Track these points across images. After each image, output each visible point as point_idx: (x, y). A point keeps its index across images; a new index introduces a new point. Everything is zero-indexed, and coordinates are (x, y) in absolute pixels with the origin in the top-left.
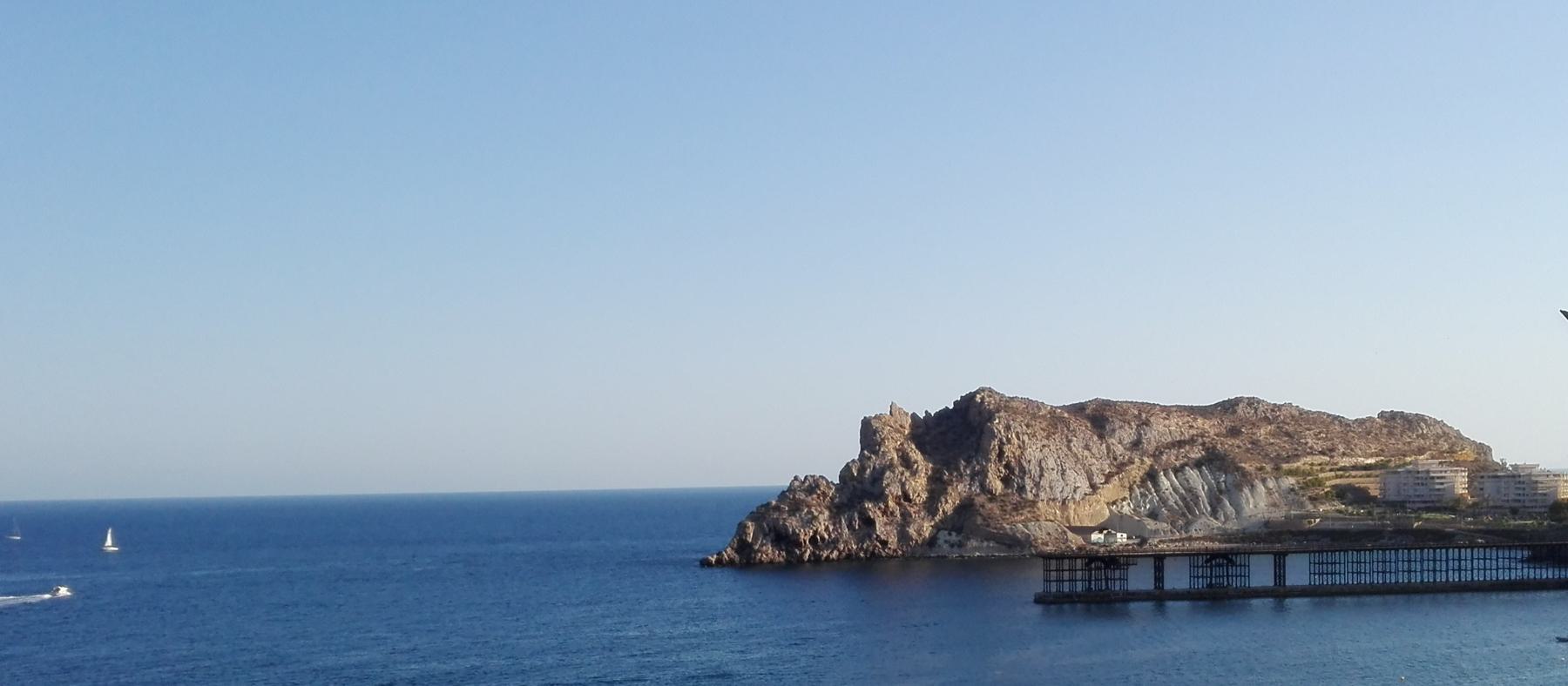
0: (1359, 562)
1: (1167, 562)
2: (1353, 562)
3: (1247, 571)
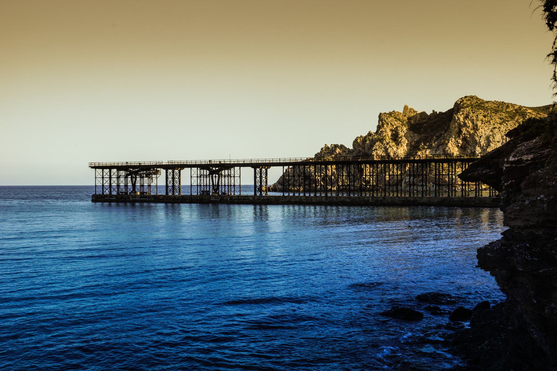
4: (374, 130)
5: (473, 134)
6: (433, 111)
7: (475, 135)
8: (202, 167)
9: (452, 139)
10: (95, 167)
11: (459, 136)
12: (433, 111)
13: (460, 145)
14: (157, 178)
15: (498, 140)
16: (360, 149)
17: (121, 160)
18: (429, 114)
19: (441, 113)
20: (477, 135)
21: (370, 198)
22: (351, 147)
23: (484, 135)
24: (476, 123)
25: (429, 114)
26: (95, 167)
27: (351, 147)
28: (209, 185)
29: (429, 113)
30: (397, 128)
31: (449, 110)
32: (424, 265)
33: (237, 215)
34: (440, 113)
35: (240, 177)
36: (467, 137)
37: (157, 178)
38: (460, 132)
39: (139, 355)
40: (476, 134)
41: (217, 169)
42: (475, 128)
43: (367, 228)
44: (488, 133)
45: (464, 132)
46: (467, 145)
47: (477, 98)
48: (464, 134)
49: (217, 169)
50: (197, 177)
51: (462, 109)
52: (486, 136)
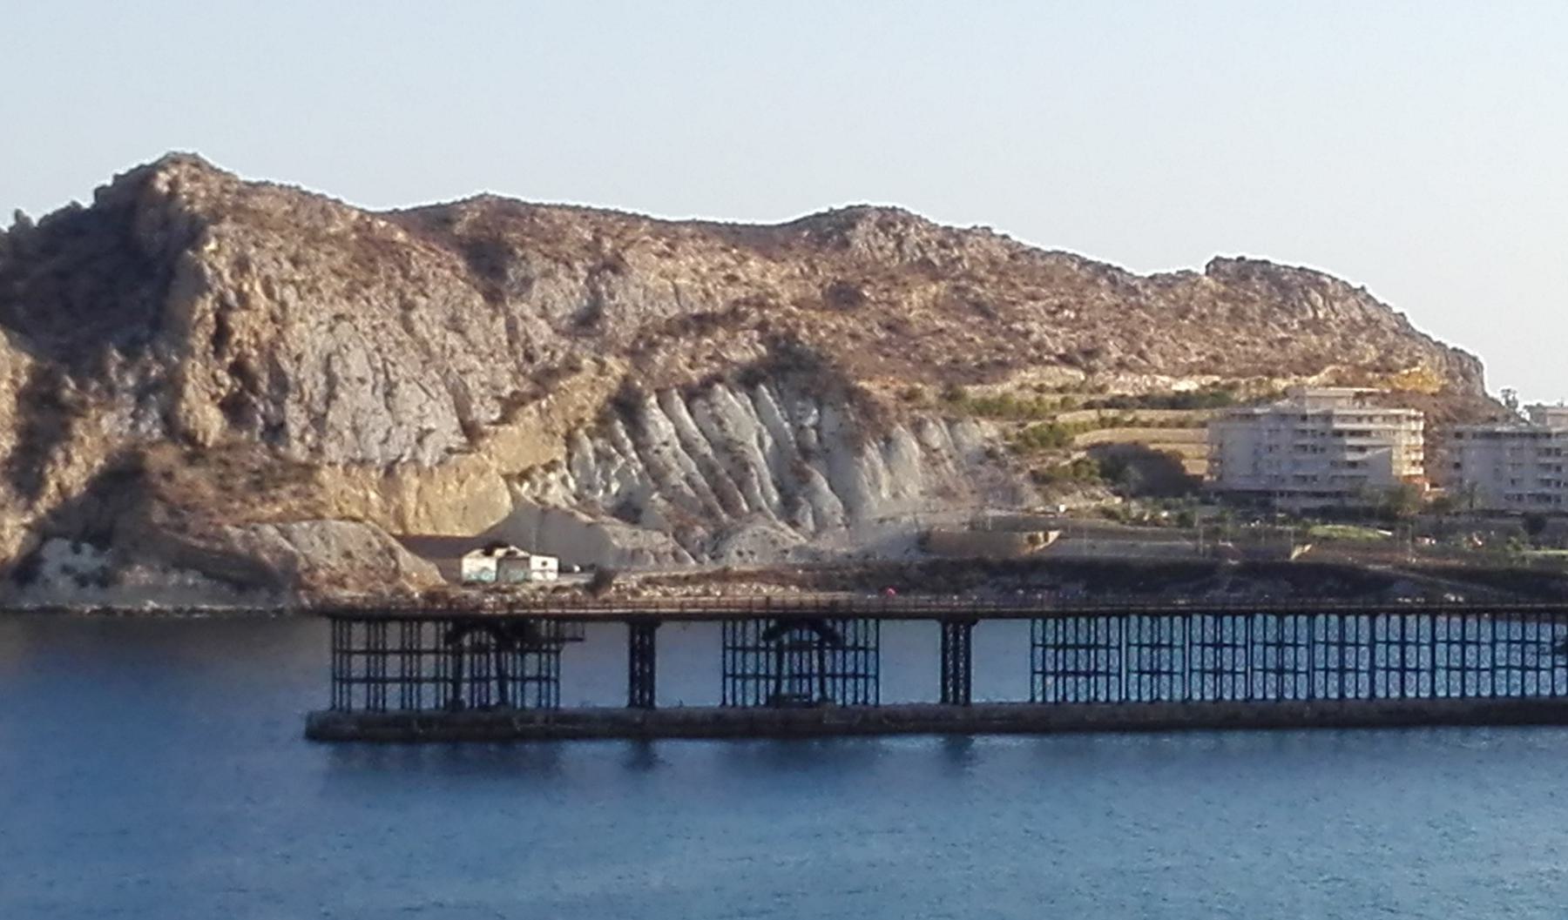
0: (1218, 645)
1: (663, 634)
2: (1140, 646)
3: (872, 662)
5: (273, 345)
6: (18, 214)
7: (278, 348)
9: (194, 366)
11: (218, 354)
12: (18, 214)
13: (223, 392)
15: (359, 375)
19: (68, 223)
20: (288, 348)
23: (309, 349)
24: (282, 296)
28: (1265, 671)
32: (1150, 355)
33: (535, 263)
36: (249, 356)
38: (221, 336)
40: (282, 345)
42: (279, 319)
44: (323, 341)
45: (237, 336)
48: (239, 343)
51: (212, 228)
52: (317, 352)
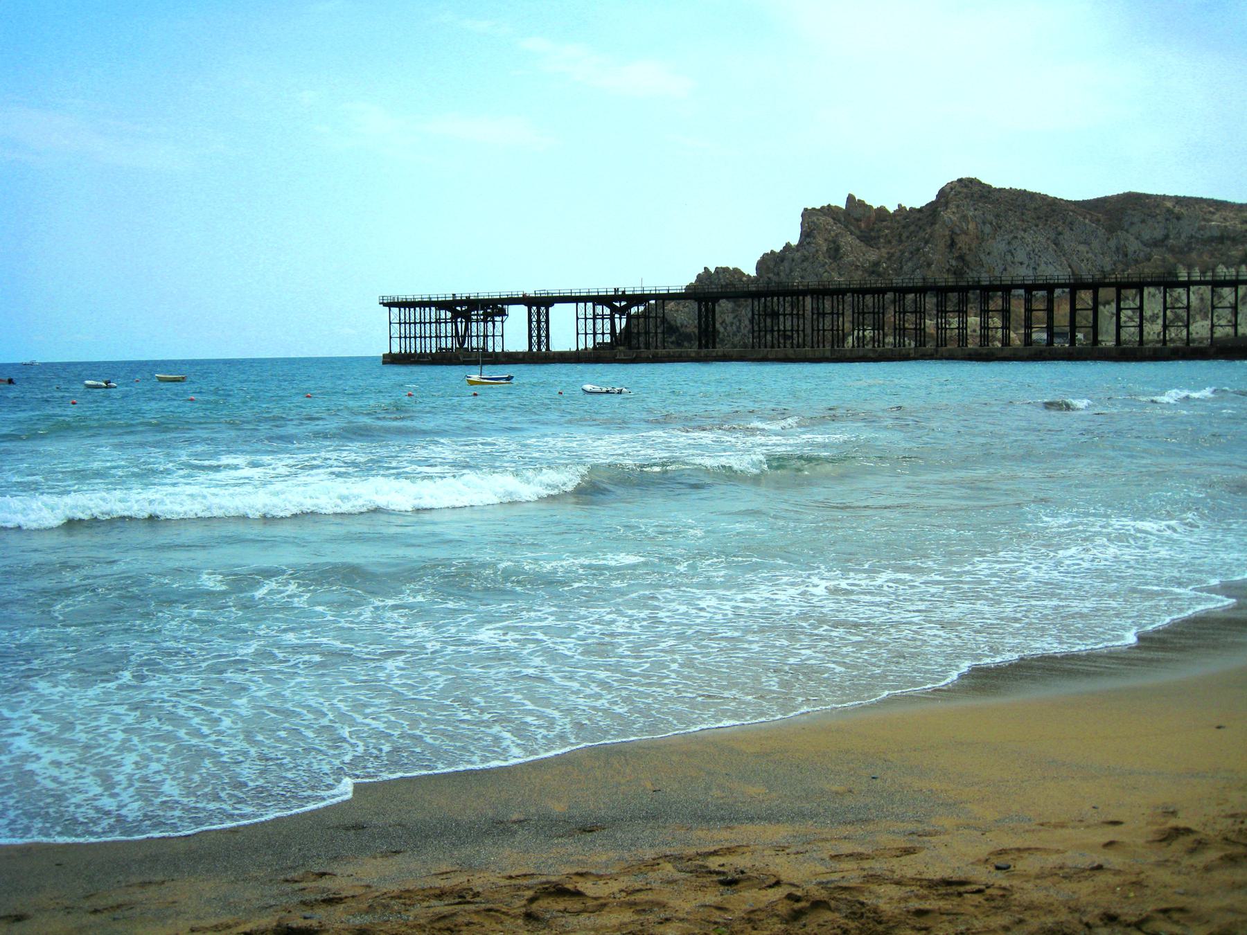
4: (795, 241)
6: (900, 205)
8: (598, 300)
10: (390, 305)
12: (900, 205)
14: (502, 322)
16: (771, 275)
17: (443, 291)
18: (892, 211)
21: (912, 351)
22: (753, 273)
25: (892, 211)
26: (390, 305)
27: (753, 273)
29: (892, 208)
30: (837, 235)
31: (1125, 195)
34: (912, 209)
35: (502, 336)
37: (502, 322)
39: (338, 644)
41: (623, 303)
43: (162, 502)
46: (965, 269)
47: (980, 183)
49: (623, 303)
50: (400, 337)
